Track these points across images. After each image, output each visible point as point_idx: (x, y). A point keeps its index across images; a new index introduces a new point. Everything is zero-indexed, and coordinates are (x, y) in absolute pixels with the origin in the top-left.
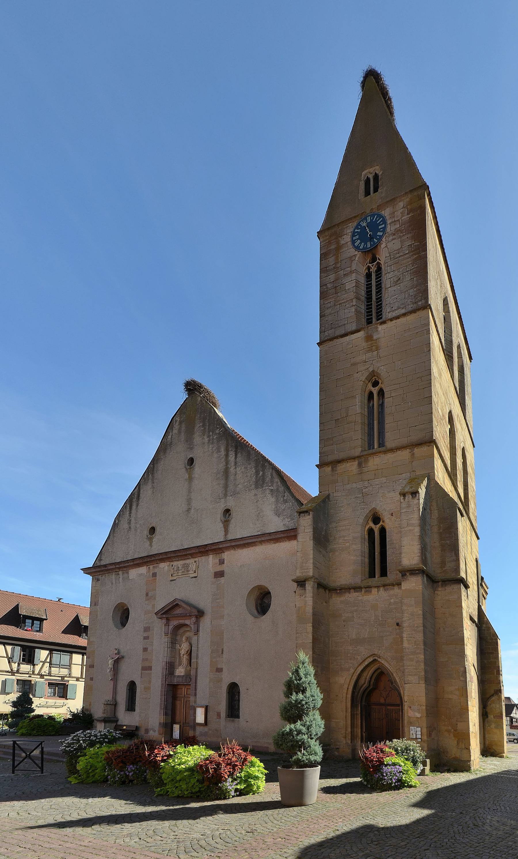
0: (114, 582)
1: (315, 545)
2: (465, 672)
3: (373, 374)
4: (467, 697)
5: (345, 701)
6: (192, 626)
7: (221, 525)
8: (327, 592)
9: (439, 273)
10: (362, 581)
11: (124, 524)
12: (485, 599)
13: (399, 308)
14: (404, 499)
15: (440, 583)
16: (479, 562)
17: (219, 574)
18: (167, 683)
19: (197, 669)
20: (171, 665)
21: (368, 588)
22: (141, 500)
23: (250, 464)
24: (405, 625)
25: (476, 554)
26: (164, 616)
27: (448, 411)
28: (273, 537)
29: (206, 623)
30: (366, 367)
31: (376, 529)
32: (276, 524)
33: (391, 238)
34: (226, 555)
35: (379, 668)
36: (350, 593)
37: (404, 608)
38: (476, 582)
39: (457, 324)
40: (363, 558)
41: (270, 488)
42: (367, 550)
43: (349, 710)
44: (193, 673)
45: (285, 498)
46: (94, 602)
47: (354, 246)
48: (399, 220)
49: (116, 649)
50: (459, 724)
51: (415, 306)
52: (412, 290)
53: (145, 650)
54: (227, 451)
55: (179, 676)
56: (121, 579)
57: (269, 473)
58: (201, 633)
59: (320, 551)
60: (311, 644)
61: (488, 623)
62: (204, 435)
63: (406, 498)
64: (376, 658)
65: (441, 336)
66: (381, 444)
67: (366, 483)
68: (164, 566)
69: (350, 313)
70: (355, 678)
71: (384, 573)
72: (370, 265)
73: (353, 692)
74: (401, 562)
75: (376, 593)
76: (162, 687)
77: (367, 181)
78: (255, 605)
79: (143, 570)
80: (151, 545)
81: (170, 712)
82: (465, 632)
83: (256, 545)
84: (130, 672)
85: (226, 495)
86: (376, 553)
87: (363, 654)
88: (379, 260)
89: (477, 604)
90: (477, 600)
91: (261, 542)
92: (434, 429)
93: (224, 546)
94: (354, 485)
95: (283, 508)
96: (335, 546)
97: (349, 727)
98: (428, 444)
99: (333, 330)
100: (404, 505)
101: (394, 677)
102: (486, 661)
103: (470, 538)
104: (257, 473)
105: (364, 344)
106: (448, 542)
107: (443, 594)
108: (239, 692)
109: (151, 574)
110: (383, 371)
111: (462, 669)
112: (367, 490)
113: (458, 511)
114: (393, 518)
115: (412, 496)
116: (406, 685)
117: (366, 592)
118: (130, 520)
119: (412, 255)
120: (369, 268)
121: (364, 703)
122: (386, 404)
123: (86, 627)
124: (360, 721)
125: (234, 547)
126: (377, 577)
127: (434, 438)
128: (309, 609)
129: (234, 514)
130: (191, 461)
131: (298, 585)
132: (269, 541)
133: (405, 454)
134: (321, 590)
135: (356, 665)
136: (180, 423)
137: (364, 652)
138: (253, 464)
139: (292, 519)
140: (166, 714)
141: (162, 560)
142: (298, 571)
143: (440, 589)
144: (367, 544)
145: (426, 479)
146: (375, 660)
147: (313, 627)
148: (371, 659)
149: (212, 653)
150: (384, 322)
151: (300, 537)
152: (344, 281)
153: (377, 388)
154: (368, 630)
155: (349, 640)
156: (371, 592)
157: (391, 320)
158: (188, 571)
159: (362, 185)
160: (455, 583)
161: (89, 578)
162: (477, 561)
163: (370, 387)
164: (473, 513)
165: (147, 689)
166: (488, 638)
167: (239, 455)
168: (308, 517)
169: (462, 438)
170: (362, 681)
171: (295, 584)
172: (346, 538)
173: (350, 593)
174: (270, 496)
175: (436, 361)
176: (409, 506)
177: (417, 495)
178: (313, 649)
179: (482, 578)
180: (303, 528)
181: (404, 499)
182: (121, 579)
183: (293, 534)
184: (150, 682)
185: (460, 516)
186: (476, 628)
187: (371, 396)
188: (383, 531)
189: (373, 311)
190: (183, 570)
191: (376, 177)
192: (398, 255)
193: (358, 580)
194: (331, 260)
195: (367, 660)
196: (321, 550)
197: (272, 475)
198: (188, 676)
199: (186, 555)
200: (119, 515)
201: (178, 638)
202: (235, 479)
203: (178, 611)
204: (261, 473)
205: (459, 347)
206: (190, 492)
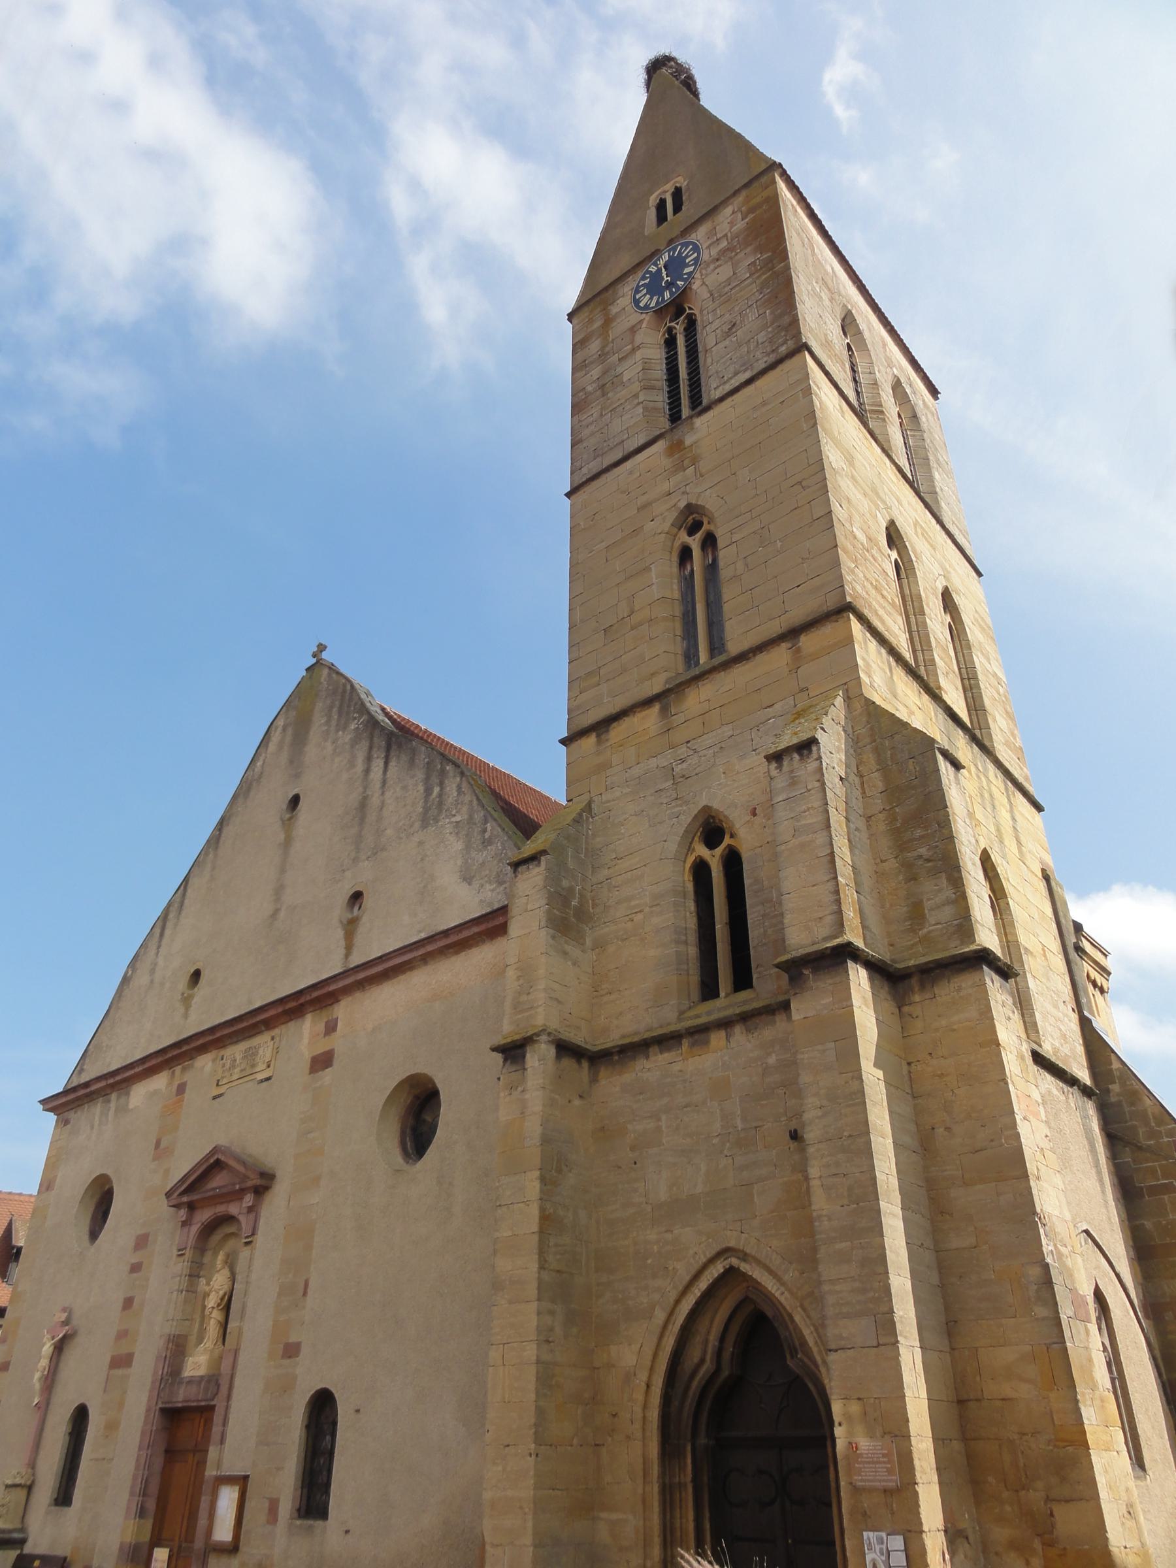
0: (96, 1126)
1: (553, 937)
2: (1048, 1282)
3: (690, 509)
4: (1073, 1386)
5: (639, 1435)
6: (242, 1219)
7: (340, 933)
8: (585, 1064)
9: (825, 281)
10: (682, 1013)
11: (142, 978)
12: (1102, 991)
13: (736, 374)
14: (780, 767)
15: (914, 981)
16: (1057, 877)
17: (322, 1062)
18: (160, 1405)
19: (236, 1352)
20: (178, 1345)
21: (699, 1033)
22: (183, 913)
23: (413, 777)
24: (811, 1135)
25: (1039, 853)
26: (185, 1199)
27: (884, 525)
28: (453, 938)
29: (277, 1208)
30: (672, 503)
31: (714, 858)
32: (464, 902)
33: (712, 266)
34: (342, 1010)
35: (745, 1300)
36: (647, 1057)
37: (805, 1078)
38: (1054, 945)
39: (885, 345)
40: (682, 948)
41: (453, 819)
42: (692, 923)
43: (655, 1470)
44: (225, 1368)
45: (487, 835)
46: (47, 1185)
47: (637, 306)
48: (726, 235)
49: (64, 1310)
50: (1058, 1510)
51: (772, 358)
52: (763, 333)
53: (128, 1303)
54: (369, 759)
55: (191, 1381)
56: (111, 1113)
57: (454, 786)
58: (259, 1239)
59: (565, 953)
60: (536, 1238)
61: (1127, 1073)
62: (326, 741)
63: (785, 763)
64: (734, 1261)
65: (842, 385)
66: (716, 645)
67: (682, 751)
68: (205, 1063)
69: (637, 408)
70: (669, 1342)
71: (743, 980)
72: (673, 324)
73: (666, 1399)
74: (784, 940)
75: (723, 1042)
76: (147, 1417)
77: (661, 205)
78: (398, 1134)
79: (160, 1082)
80: (186, 1016)
81: (151, 1505)
82: (1023, 1129)
83: (411, 969)
84: (82, 1381)
85: (356, 860)
86: (718, 927)
87: (691, 1252)
88: (690, 309)
89: (1075, 1017)
90: (1071, 1004)
91: (425, 959)
92: (848, 578)
93: (341, 984)
94: (653, 763)
95: (481, 861)
96: (606, 930)
97: (657, 1540)
98: (834, 618)
99: (599, 459)
100: (780, 783)
101: (796, 1327)
102: (1148, 1224)
103: (1008, 816)
104: (428, 791)
105: (667, 462)
106: (923, 851)
107: (940, 1004)
108: (335, 1423)
109: (175, 1087)
110: (710, 501)
111: (1035, 1272)
112: (684, 765)
113: (940, 758)
114: (758, 820)
115: (801, 755)
116: (832, 1357)
117: (692, 1045)
118: (156, 964)
119: (758, 277)
120: (670, 330)
121: (702, 1440)
122: (721, 563)
123: (19, 1250)
124: (691, 1515)
125: (361, 985)
126: (722, 994)
127: (849, 599)
128: (533, 1128)
129: (368, 901)
130: (295, 801)
131: (505, 1060)
132: (444, 952)
133: (780, 656)
134: (568, 1063)
135: (673, 1296)
136: (284, 729)
137: (691, 1248)
138: (420, 775)
139: (500, 883)
140: (142, 1513)
141: (203, 1049)
142: (506, 1021)
143: (917, 998)
144: (691, 905)
145: (839, 701)
146: (731, 1271)
147: (543, 1180)
148: (718, 1269)
149: (280, 1295)
150: (708, 408)
151: (514, 929)
152: (619, 370)
153: (699, 536)
154: (703, 1167)
155: (649, 1208)
156: (707, 1042)
157: (722, 399)
158: (253, 1066)
159: (652, 214)
160: (961, 971)
161: (52, 1118)
162: (1047, 878)
163: (684, 537)
164: (1007, 744)
165: (111, 1427)
166: (1141, 1131)
167: (393, 763)
168: (537, 870)
169: (935, 564)
170: (694, 1354)
171: (499, 1057)
172: (633, 903)
173: (647, 1057)
174: (452, 838)
175: (833, 439)
176: (793, 782)
177: (814, 748)
178: (541, 1252)
179: (1078, 927)
180: (524, 900)
181: (780, 767)
182: (111, 1113)
183: (501, 920)
184: (121, 1405)
185: (951, 769)
186: (1090, 1108)
187: (685, 554)
188: (733, 861)
189: (685, 393)
190: (243, 1066)
191: (677, 194)
192: (727, 289)
193: (667, 1018)
194: (595, 346)
195: (707, 1273)
196: (568, 948)
197: (459, 788)
198: (212, 1381)
199: (255, 1025)
200: (136, 957)
201: (207, 1259)
202: (380, 819)
203: (218, 1181)
204: (436, 790)
205: (897, 386)
206: (283, 870)
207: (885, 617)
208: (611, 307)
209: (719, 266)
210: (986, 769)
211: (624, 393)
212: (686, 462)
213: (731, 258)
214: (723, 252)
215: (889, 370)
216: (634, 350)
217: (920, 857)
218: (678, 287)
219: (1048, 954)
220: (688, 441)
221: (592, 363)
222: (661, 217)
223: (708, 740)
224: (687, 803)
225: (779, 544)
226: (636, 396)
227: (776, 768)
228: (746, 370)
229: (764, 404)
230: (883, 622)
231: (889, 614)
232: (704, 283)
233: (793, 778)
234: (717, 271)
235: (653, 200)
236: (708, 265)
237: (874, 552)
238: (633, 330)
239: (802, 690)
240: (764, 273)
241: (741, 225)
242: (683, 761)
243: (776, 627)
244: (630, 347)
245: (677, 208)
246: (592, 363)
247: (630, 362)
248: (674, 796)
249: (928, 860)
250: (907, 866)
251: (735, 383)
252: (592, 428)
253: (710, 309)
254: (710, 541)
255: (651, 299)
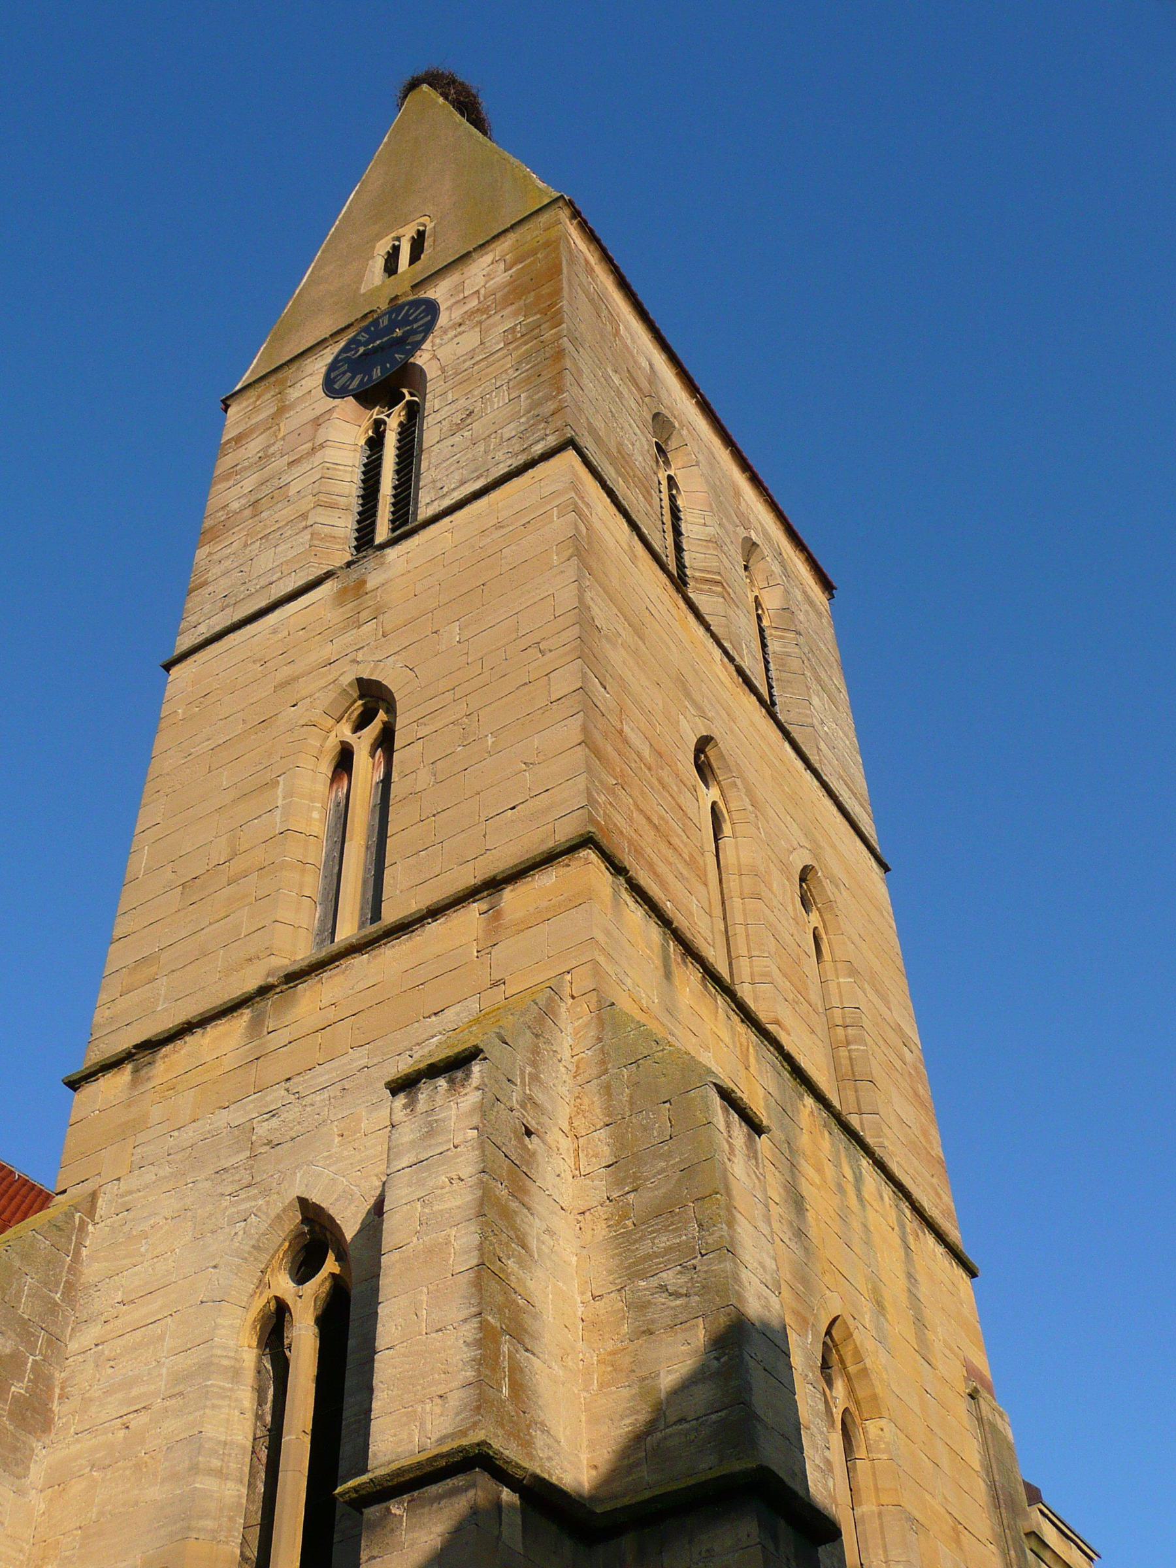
14: (411, 1105)
30: (331, 678)
33: (451, 333)
51: (521, 459)
52: (512, 425)
63: (422, 1097)
77: (392, 257)
98: (565, 859)
105: (334, 616)
106: (670, 1277)
152: (286, 479)
159: (379, 263)
172: (135, 1392)
176: (431, 1131)
181: (411, 1105)
187: (344, 761)
207: (670, 878)
208: (291, 390)
209: (460, 334)
210: (858, 1179)
211: (287, 512)
212: (364, 615)
213: (480, 323)
214: (472, 313)
215: (740, 530)
216: (313, 450)
217: (663, 1288)
218: (394, 361)
219: (966, 1538)
220: (372, 582)
221: (246, 469)
222: (391, 265)
223: (323, 1076)
224: (266, 1192)
225: (490, 740)
226: (304, 516)
227: (405, 1107)
228: (478, 477)
229: (499, 526)
230: (663, 884)
231: (680, 877)
232: (435, 356)
233: (430, 1123)
234: (456, 340)
235: (383, 247)
236: (445, 332)
237: (664, 774)
238: (317, 422)
239: (495, 984)
240: (526, 343)
241: (502, 277)
242: (273, 1114)
243: (469, 877)
244: (310, 445)
245: (414, 257)
246: (246, 469)
247: (305, 466)
248: (247, 1179)
249: (676, 1295)
250: (639, 1306)
251: (458, 495)
252: (227, 564)
253: (438, 391)
254: (386, 742)
255: (352, 378)
